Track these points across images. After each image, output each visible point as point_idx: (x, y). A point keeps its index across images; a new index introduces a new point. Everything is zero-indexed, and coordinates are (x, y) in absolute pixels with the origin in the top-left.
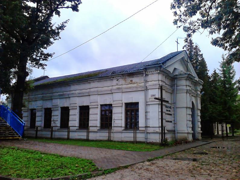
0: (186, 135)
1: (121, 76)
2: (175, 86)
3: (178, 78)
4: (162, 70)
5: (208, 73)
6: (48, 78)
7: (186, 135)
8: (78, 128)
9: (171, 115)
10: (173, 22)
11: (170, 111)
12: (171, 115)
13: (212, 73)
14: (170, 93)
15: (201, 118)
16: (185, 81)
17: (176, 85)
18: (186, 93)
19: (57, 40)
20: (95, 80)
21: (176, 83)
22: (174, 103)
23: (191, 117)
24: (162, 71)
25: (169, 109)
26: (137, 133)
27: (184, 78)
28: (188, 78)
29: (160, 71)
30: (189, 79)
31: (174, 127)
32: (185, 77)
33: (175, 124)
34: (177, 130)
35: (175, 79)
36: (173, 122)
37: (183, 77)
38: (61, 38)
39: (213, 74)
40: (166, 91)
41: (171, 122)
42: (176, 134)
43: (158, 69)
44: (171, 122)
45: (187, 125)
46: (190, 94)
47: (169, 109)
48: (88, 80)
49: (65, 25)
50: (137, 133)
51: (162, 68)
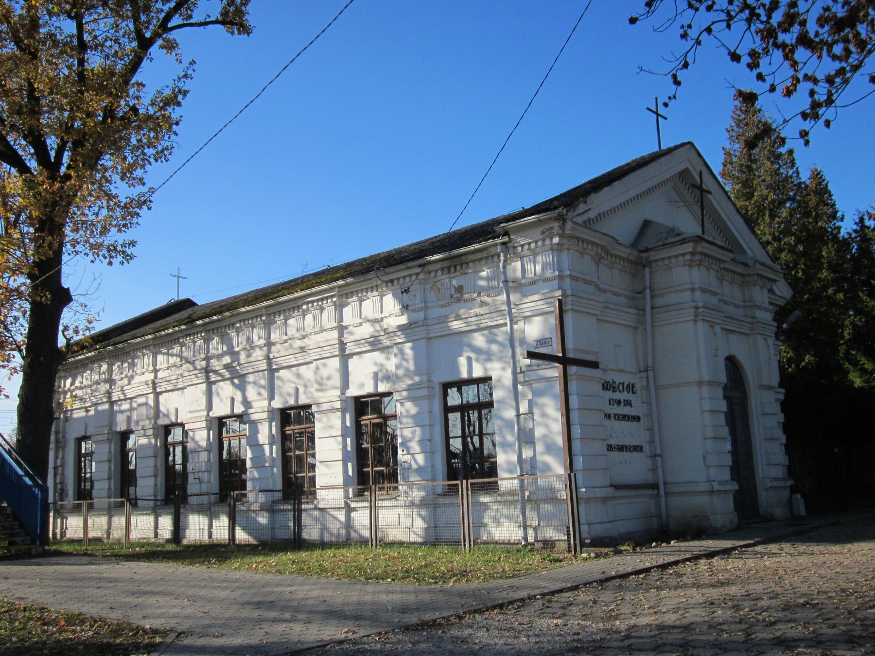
0: (705, 500)
1: (417, 274)
2: (644, 298)
3: (657, 261)
4: (568, 232)
5: (839, 228)
6: (195, 308)
7: (705, 500)
8: (279, 495)
9: (637, 419)
10: (248, 34)
11: (628, 403)
12: (637, 419)
13: (850, 231)
14: (631, 326)
15: (784, 433)
16: (687, 268)
17: (648, 291)
18: (695, 321)
19: (795, 155)
20: (327, 298)
21: (648, 284)
22: (646, 370)
23: (723, 422)
24: (571, 237)
25: (623, 396)
26: (110, 443)
27: (680, 259)
28: (698, 257)
29: (561, 236)
30: (701, 261)
31: (654, 470)
32: (683, 255)
33: (654, 456)
34: (665, 483)
35: (644, 266)
36: (646, 448)
37: (676, 256)
38: (807, 148)
39: (855, 231)
40: (598, 320)
41: (638, 449)
42: (663, 499)
43: (552, 228)
44: (638, 449)
45: (704, 458)
46: (712, 325)
47: (623, 396)
48: (300, 303)
49: (185, 88)
50: (110, 443)
51: (569, 225)
